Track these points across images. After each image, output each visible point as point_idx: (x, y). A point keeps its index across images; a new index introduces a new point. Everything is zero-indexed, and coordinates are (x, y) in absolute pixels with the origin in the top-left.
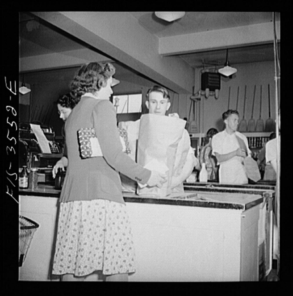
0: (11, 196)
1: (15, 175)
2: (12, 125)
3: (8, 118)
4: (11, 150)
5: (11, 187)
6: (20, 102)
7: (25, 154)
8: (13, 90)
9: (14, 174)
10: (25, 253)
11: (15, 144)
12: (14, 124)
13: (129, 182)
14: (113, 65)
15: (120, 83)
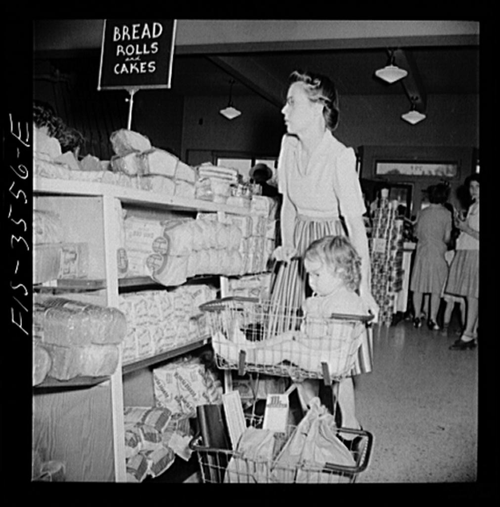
5: (18, 309)
9: (19, 286)
10: (46, 446)
11: (25, 230)
13: (144, 466)
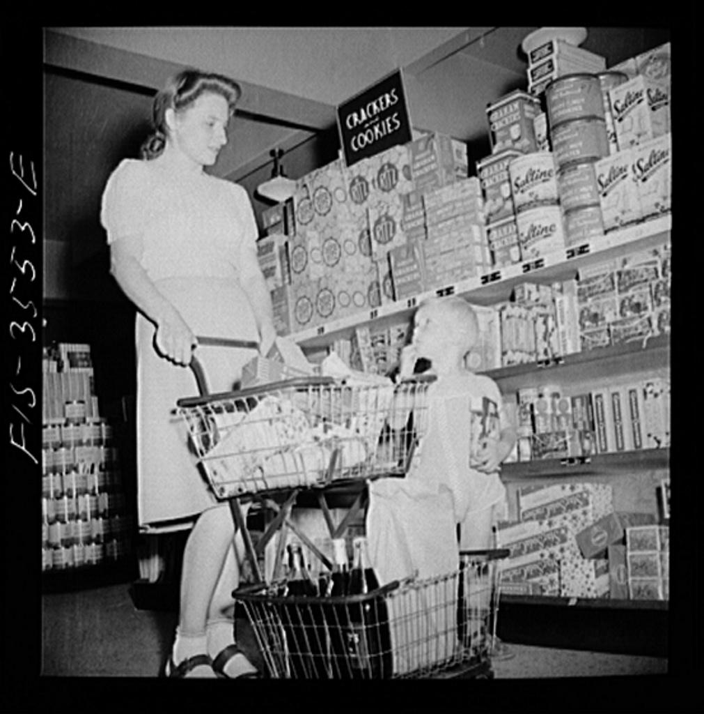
0: (23, 448)
1: (28, 392)
2: (23, 329)
3: (15, 280)
4: (23, 270)
6: (44, 61)
7: (45, 322)
8: (28, 178)
9: (25, 391)
12: (27, 327)
14: (241, 184)
15: (257, 185)
